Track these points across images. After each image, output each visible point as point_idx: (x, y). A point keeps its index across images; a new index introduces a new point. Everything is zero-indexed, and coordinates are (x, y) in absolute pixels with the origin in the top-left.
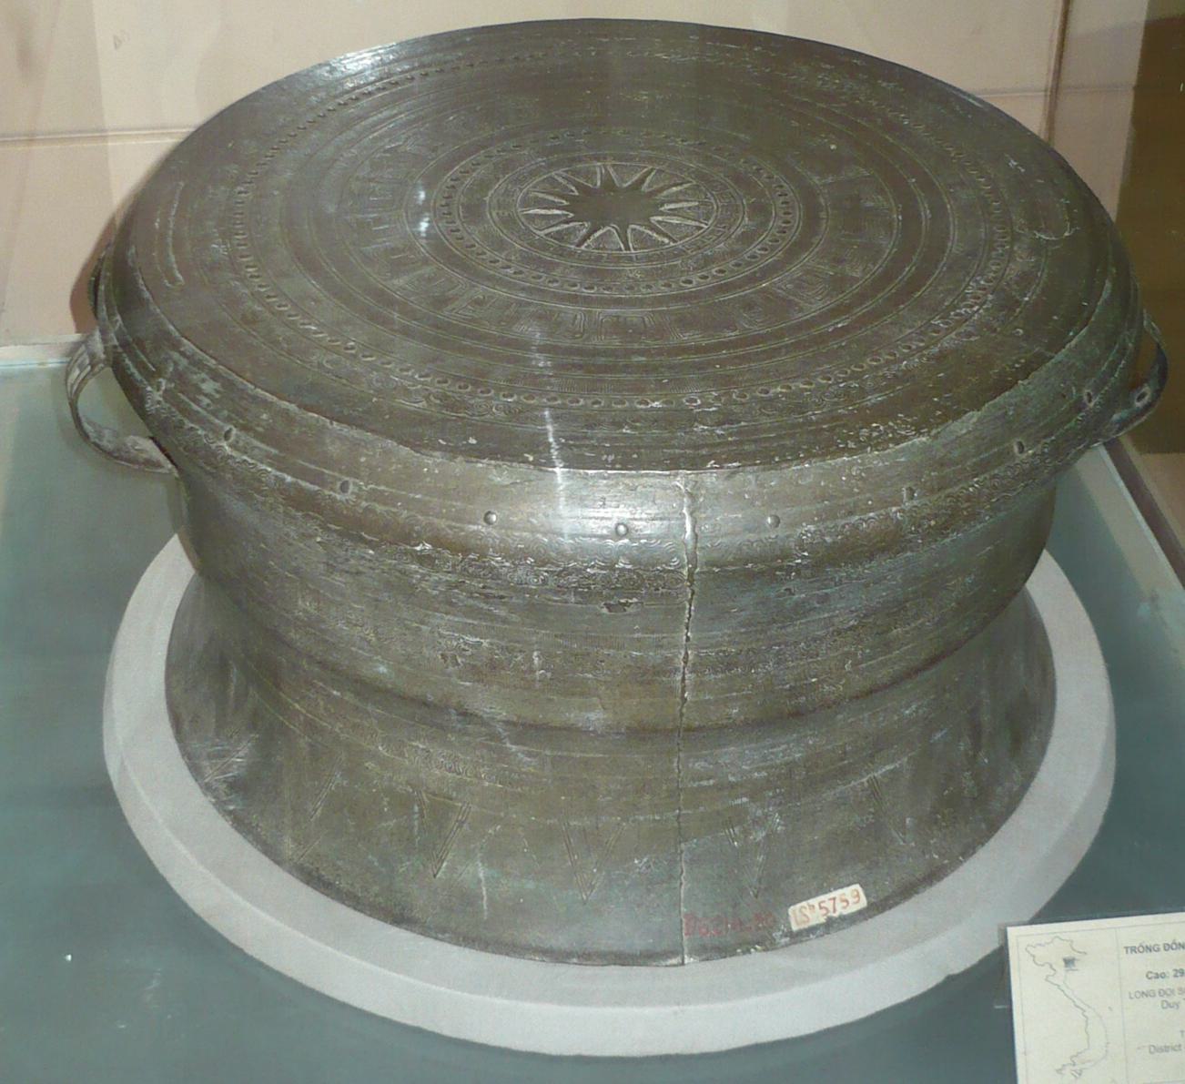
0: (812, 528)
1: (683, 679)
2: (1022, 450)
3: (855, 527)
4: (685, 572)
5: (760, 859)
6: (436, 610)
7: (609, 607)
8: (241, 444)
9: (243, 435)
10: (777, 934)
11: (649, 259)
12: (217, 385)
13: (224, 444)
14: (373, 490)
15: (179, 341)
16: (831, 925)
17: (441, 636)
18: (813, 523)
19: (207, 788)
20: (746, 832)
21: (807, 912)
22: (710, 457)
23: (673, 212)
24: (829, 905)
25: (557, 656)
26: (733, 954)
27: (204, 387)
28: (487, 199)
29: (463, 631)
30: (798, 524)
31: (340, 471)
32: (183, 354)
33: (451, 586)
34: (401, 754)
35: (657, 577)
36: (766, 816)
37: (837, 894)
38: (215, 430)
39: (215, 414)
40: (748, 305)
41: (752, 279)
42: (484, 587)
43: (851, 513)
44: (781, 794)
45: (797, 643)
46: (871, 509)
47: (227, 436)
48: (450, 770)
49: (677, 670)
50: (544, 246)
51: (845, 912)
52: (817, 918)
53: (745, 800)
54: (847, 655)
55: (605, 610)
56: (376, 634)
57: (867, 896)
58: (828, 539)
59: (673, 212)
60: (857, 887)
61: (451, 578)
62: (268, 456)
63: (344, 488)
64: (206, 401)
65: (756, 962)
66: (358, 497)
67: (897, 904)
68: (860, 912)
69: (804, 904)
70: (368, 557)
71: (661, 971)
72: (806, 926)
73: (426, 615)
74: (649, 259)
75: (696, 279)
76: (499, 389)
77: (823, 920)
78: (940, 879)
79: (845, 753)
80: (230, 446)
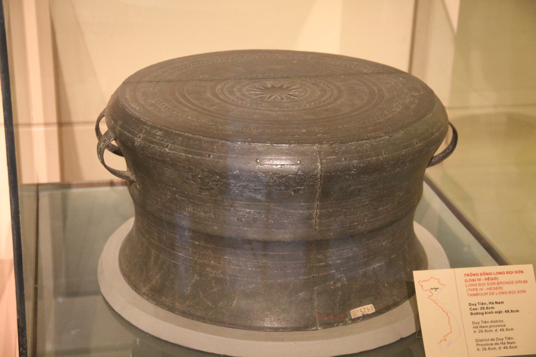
0: (356, 161)
1: (316, 222)
2: (417, 144)
3: (369, 162)
4: (319, 175)
5: (340, 293)
6: (237, 200)
7: (294, 191)
8: (173, 148)
9: (173, 145)
12: (162, 132)
13: (167, 149)
16: (365, 317)
17: (238, 211)
18: (356, 159)
19: (142, 294)
20: (335, 283)
21: (356, 312)
24: (363, 310)
26: (333, 326)
27: (157, 134)
29: (245, 208)
30: (352, 160)
31: (208, 151)
32: (148, 126)
33: (245, 187)
34: (220, 263)
35: (311, 177)
39: (162, 141)
42: (255, 186)
43: (368, 157)
44: (345, 270)
45: (350, 209)
46: (374, 156)
47: (167, 147)
48: (237, 266)
49: (314, 218)
51: (369, 313)
52: (360, 314)
53: (334, 271)
54: (366, 215)
55: (293, 193)
56: (214, 214)
57: (375, 308)
58: (361, 165)
60: (371, 305)
61: (244, 184)
62: (182, 150)
64: (158, 137)
65: (341, 328)
66: (214, 158)
67: (385, 312)
68: (373, 313)
71: (309, 332)
73: (233, 203)
75: (307, 106)
77: (361, 315)
78: (398, 306)
79: (365, 256)
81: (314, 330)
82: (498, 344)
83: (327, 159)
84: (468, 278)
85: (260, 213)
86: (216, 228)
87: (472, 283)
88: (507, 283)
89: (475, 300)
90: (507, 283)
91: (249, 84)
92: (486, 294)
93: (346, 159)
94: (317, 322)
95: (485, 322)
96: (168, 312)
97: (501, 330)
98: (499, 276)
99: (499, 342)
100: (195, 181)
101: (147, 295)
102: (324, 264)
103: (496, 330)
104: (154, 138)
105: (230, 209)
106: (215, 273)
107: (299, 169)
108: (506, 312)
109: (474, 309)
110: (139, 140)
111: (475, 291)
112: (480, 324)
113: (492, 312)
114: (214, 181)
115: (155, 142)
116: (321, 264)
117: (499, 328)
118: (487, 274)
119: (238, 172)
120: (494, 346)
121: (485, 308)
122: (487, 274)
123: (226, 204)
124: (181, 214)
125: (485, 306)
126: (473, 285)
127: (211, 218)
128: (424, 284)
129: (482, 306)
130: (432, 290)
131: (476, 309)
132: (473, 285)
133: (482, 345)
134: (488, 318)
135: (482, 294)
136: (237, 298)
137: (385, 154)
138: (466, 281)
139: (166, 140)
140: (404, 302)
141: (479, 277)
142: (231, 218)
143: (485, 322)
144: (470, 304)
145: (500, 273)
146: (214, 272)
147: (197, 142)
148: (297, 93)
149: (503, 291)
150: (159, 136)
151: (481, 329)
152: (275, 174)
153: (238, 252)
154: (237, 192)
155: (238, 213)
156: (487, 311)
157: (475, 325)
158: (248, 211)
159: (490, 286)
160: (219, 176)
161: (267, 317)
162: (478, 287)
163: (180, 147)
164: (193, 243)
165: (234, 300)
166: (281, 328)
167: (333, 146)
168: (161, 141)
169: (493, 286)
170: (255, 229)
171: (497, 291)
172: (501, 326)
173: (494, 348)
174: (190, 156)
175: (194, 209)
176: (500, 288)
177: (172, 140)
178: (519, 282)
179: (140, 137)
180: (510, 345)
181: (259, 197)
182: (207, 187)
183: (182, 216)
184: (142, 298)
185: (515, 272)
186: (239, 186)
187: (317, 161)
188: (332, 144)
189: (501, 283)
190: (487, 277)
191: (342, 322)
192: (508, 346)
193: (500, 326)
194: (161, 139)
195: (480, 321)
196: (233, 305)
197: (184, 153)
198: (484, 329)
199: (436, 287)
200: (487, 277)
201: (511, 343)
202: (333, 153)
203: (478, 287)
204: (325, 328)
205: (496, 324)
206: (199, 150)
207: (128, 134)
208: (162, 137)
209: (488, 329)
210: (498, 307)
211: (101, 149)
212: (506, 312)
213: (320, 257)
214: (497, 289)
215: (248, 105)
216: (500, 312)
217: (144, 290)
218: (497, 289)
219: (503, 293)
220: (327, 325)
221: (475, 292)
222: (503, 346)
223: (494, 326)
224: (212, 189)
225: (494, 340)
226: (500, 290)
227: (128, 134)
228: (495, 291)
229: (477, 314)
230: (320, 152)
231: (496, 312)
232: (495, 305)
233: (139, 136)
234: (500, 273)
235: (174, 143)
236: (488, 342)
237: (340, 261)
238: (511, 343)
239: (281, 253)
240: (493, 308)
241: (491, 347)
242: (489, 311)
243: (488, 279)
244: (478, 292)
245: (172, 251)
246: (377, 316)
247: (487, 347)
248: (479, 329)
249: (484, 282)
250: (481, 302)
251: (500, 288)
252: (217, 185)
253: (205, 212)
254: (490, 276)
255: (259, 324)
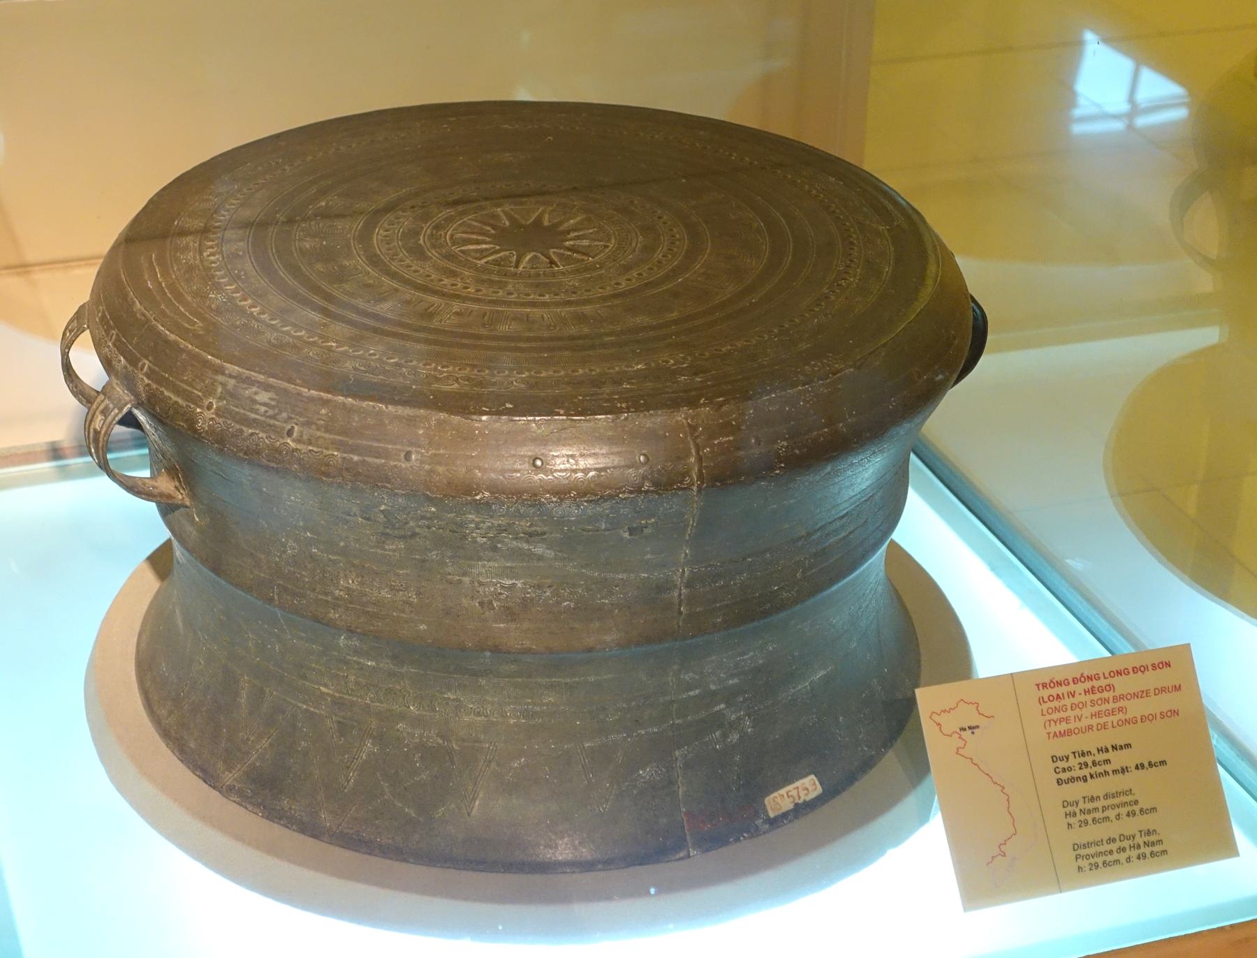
1: (680, 595)
5: (737, 758)
6: (480, 559)
7: (632, 531)
8: (305, 437)
10: (759, 822)
11: (578, 271)
14: (435, 455)
15: (223, 367)
16: (801, 809)
17: (481, 584)
19: (227, 791)
20: (725, 736)
21: (780, 800)
22: (701, 396)
23: (578, 238)
24: (794, 793)
25: (580, 586)
26: (727, 843)
28: (421, 242)
29: (501, 576)
30: (775, 442)
32: (231, 376)
33: (501, 529)
36: (739, 719)
37: (798, 784)
38: (278, 432)
39: (273, 417)
40: (675, 294)
41: (667, 278)
42: (531, 525)
47: (290, 433)
48: (479, 714)
49: (675, 586)
50: (484, 270)
52: (787, 805)
53: (722, 706)
55: (626, 535)
56: (418, 594)
59: (578, 238)
60: (813, 777)
61: (502, 521)
62: (333, 442)
63: (408, 456)
64: (263, 409)
66: (422, 462)
69: (776, 794)
70: (428, 515)
71: (669, 864)
72: (780, 812)
73: (470, 566)
74: (578, 271)
76: (511, 370)
77: (791, 806)
80: (293, 441)
81: (682, 859)
82: (1124, 850)
83: (712, 446)
84: (1045, 693)
85: (539, 587)
86: (423, 627)
87: (1056, 704)
88: (1135, 695)
89: (1064, 746)
90: (1135, 695)
91: (450, 220)
92: (1090, 728)
93: (758, 442)
94: (688, 838)
95: (1092, 799)
96: (302, 836)
97: (1128, 815)
98: (1115, 681)
99: (1126, 844)
100: (368, 519)
101: (240, 793)
102: (697, 692)
103: (1118, 817)
104: (252, 410)
105: (460, 582)
106: (421, 736)
107: (644, 478)
108: (1137, 767)
109: (1064, 770)
110: (209, 415)
111: (1064, 724)
112: (1081, 805)
113: (1106, 773)
114: (423, 518)
115: (255, 420)
116: (692, 693)
117: (1123, 811)
118: (1090, 678)
119: (487, 494)
120: (1115, 856)
121: (1090, 764)
122: (1090, 678)
123: (450, 569)
124: (326, 594)
125: (1089, 759)
126: (1057, 710)
127: (410, 604)
128: (942, 719)
129: (1082, 760)
130: (963, 733)
131: (1070, 769)
132: (1057, 710)
133: (1087, 857)
134: (1096, 787)
135: (1080, 731)
136: (481, 795)
137: (851, 416)
138: (1041, 701)
139: (284, 415)
140: (884, 754)
141: (1072, 687)
142: (464, 601)
143: (1092, 799)
144: (1054, 759)
145: (1119, 673)
146: (417, 732)
147: (370, 421)
148: (586, 243)
149: (1128, 717)
150: (264, 404)
151: (1082, 817)
152: (585, 494)
153: (483, 682)
154: (481, 540)
155: (481, 589)
156: (1093, 770)
157: (1069, 809)
158: (508, 582)
159: (1097, 708)
160: (435, 506)
161: (562, 838)
162: (1069, 713)
163: (327, 436)
164: (359, 663)
165: (474, 799)
166: (599, 862)
167: (724, 408)
168: (270, 417)
169: (1104, 707)
170: (526, 625)
171: (1115, 719)
172: (1129, 804)
173: (1117, 862)
174: (356, 458)
175: (362, 584)
176: (1120, 710)
177: (301, 415)
178: (1163, 690)
179: (209, 407)
180: (1151, 849)
181: (539, 550)
182: (402, 533)
183: (329, 598)
184: (225, 800)
185: (1153, 665)
186: (489, 528)
187: (688, 455)
188: (721, 405)
189: (1122, 697)
190: (1088, 685)
191: (748, 832)
192: (1147, 850)
193: (1124, 804)
194: (271, 412)
195: (1079, 797)
196: (474, 812)
197: (338, 450)
198: (1089, 818)
199: (973, 724)
200: (1088, 685)
201: (1153, 844)
202: (726, 428)
203: (1069, 713)
204: (708, 850)
205: (1116, 801)
206: (379, 441)
207: (174, 398)
208: (273, 407)
209: (1098, 815)
210: (1118, 759)
211: (97, 433)
212: (1137, 767)
213: (688, 677)
214: (1113, 712)
215: (471, 290)
216: (1124, 770)
217: (229, 778)
218: (1113, 712)
219: (1127, 722)
220: (712, 841)
221: (1063, 727)
222: (1134, 853)
223: (1113, 807)
224: (414, 535)
225: (1114, 840)
226: (1121, 716)
227: (174, 398)
228: (1111, 718)
229: (1072, 780)
230: (693, 428)
231: (1115, 772)
232: (1111, 755)
233: (206, 403)
234: (1119, 673)
235: (308, 424)
236: (1101, 849)
237: (736, 681)
238: (1153, 844)
239: (592, 679)
240: (1107, 761)
241: (1109, 858)
242: (1099, 769)
243: (1092, 690)
244: (1071, 726)
245: (300, 682)
246: (827, 801)
247: (1100, 860)
248: (1079, 817)
249: (1083, 698)
250: (1078, 748)
251: (1120, 710)
252: (429, 527)
253: (392, 589)
254: (1096, 683)
255: (549, 855)
